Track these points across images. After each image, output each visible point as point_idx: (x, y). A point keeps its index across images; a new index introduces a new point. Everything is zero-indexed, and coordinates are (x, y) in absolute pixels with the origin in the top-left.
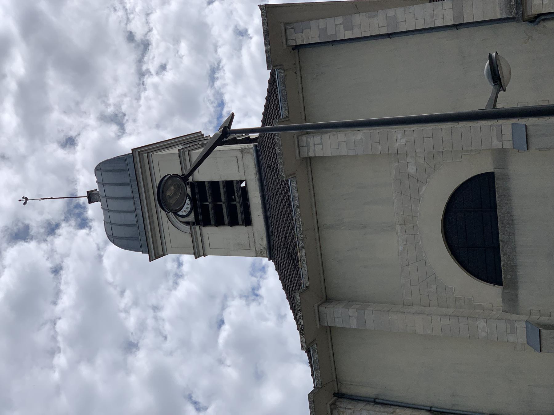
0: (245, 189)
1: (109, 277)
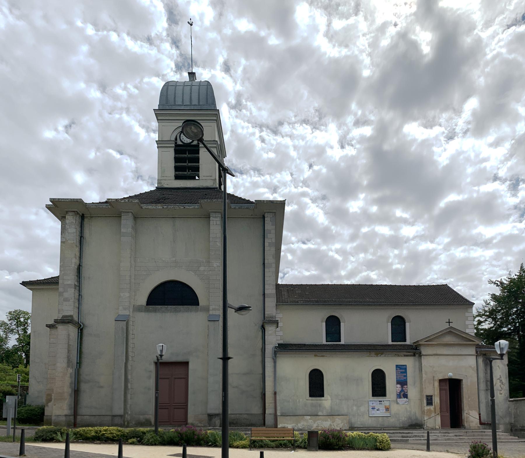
0: (194, 178)
1: (146, 80)
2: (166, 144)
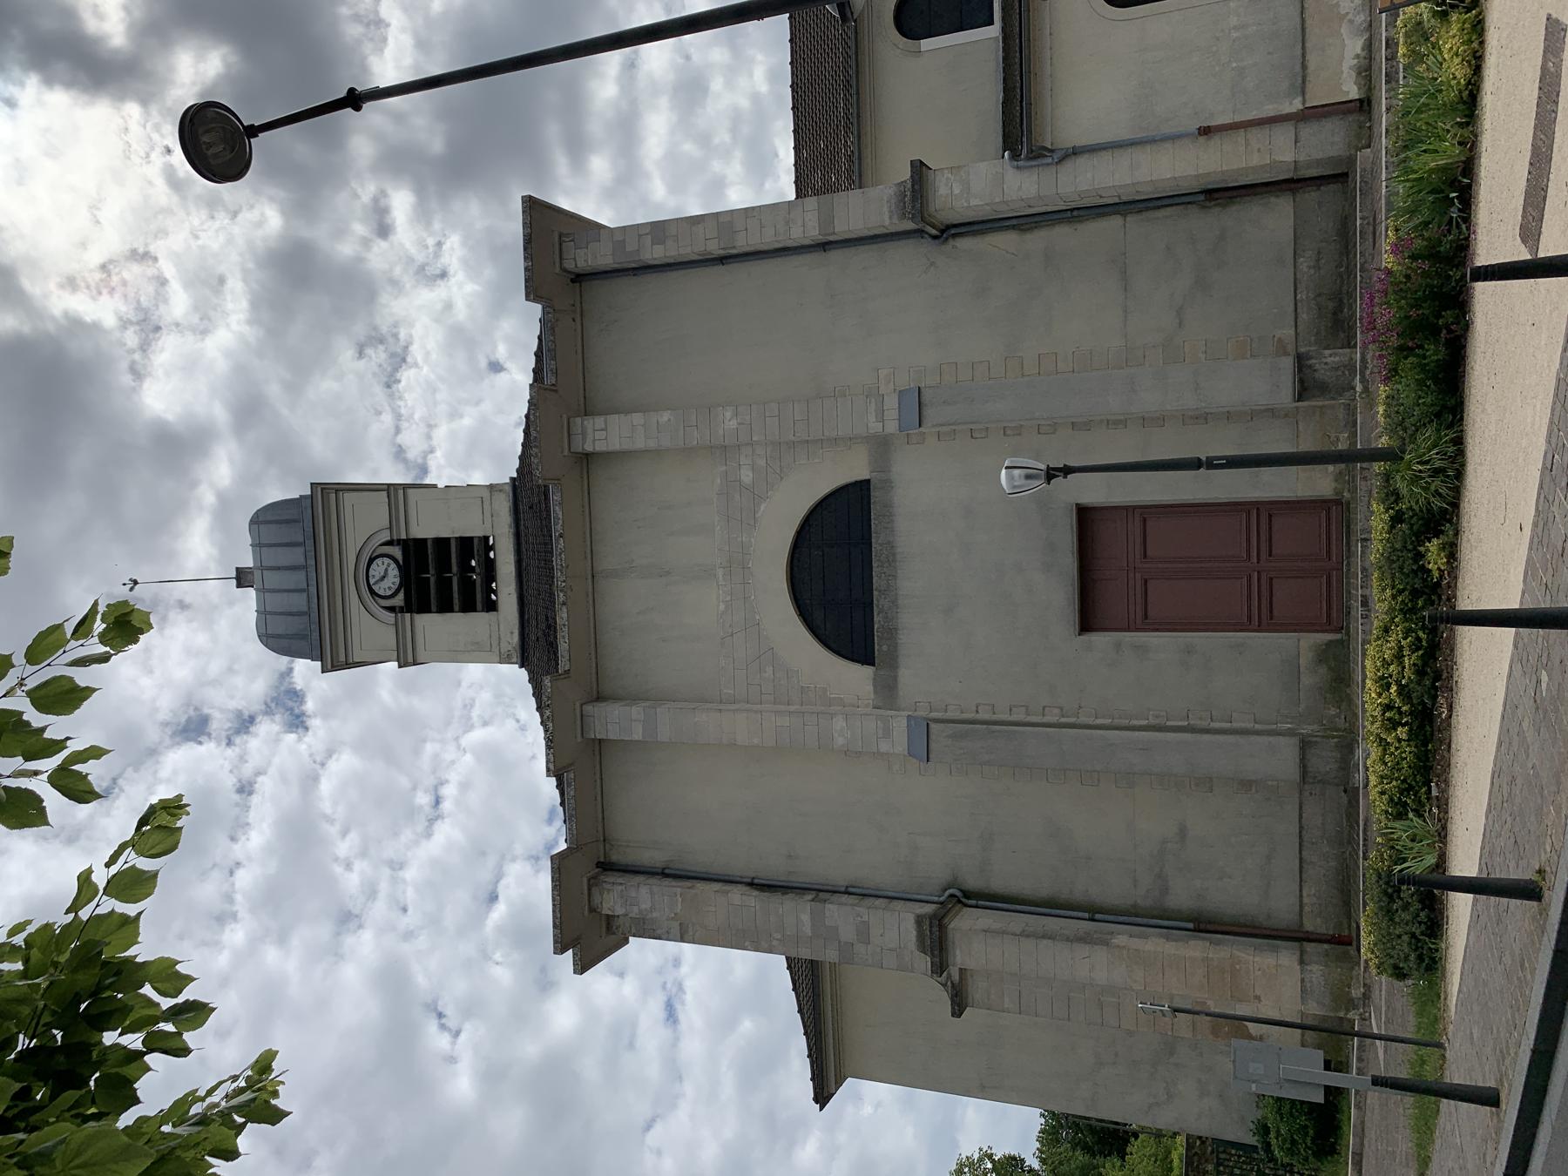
1: (326, 807)
2: (404, 637)
